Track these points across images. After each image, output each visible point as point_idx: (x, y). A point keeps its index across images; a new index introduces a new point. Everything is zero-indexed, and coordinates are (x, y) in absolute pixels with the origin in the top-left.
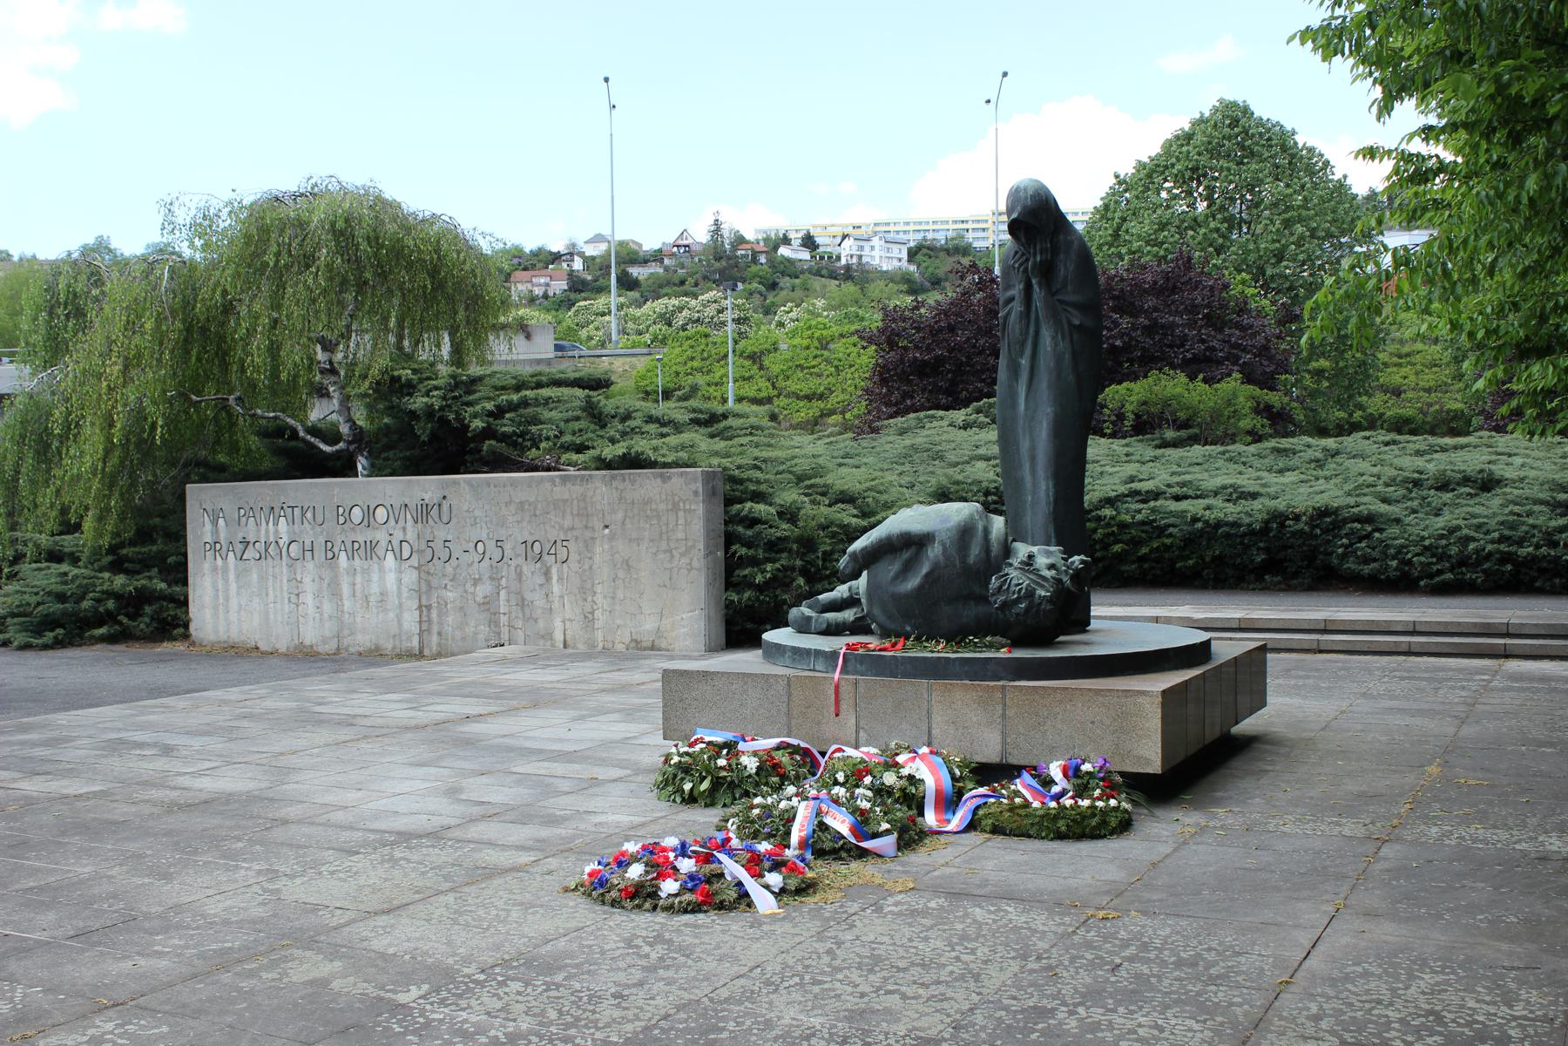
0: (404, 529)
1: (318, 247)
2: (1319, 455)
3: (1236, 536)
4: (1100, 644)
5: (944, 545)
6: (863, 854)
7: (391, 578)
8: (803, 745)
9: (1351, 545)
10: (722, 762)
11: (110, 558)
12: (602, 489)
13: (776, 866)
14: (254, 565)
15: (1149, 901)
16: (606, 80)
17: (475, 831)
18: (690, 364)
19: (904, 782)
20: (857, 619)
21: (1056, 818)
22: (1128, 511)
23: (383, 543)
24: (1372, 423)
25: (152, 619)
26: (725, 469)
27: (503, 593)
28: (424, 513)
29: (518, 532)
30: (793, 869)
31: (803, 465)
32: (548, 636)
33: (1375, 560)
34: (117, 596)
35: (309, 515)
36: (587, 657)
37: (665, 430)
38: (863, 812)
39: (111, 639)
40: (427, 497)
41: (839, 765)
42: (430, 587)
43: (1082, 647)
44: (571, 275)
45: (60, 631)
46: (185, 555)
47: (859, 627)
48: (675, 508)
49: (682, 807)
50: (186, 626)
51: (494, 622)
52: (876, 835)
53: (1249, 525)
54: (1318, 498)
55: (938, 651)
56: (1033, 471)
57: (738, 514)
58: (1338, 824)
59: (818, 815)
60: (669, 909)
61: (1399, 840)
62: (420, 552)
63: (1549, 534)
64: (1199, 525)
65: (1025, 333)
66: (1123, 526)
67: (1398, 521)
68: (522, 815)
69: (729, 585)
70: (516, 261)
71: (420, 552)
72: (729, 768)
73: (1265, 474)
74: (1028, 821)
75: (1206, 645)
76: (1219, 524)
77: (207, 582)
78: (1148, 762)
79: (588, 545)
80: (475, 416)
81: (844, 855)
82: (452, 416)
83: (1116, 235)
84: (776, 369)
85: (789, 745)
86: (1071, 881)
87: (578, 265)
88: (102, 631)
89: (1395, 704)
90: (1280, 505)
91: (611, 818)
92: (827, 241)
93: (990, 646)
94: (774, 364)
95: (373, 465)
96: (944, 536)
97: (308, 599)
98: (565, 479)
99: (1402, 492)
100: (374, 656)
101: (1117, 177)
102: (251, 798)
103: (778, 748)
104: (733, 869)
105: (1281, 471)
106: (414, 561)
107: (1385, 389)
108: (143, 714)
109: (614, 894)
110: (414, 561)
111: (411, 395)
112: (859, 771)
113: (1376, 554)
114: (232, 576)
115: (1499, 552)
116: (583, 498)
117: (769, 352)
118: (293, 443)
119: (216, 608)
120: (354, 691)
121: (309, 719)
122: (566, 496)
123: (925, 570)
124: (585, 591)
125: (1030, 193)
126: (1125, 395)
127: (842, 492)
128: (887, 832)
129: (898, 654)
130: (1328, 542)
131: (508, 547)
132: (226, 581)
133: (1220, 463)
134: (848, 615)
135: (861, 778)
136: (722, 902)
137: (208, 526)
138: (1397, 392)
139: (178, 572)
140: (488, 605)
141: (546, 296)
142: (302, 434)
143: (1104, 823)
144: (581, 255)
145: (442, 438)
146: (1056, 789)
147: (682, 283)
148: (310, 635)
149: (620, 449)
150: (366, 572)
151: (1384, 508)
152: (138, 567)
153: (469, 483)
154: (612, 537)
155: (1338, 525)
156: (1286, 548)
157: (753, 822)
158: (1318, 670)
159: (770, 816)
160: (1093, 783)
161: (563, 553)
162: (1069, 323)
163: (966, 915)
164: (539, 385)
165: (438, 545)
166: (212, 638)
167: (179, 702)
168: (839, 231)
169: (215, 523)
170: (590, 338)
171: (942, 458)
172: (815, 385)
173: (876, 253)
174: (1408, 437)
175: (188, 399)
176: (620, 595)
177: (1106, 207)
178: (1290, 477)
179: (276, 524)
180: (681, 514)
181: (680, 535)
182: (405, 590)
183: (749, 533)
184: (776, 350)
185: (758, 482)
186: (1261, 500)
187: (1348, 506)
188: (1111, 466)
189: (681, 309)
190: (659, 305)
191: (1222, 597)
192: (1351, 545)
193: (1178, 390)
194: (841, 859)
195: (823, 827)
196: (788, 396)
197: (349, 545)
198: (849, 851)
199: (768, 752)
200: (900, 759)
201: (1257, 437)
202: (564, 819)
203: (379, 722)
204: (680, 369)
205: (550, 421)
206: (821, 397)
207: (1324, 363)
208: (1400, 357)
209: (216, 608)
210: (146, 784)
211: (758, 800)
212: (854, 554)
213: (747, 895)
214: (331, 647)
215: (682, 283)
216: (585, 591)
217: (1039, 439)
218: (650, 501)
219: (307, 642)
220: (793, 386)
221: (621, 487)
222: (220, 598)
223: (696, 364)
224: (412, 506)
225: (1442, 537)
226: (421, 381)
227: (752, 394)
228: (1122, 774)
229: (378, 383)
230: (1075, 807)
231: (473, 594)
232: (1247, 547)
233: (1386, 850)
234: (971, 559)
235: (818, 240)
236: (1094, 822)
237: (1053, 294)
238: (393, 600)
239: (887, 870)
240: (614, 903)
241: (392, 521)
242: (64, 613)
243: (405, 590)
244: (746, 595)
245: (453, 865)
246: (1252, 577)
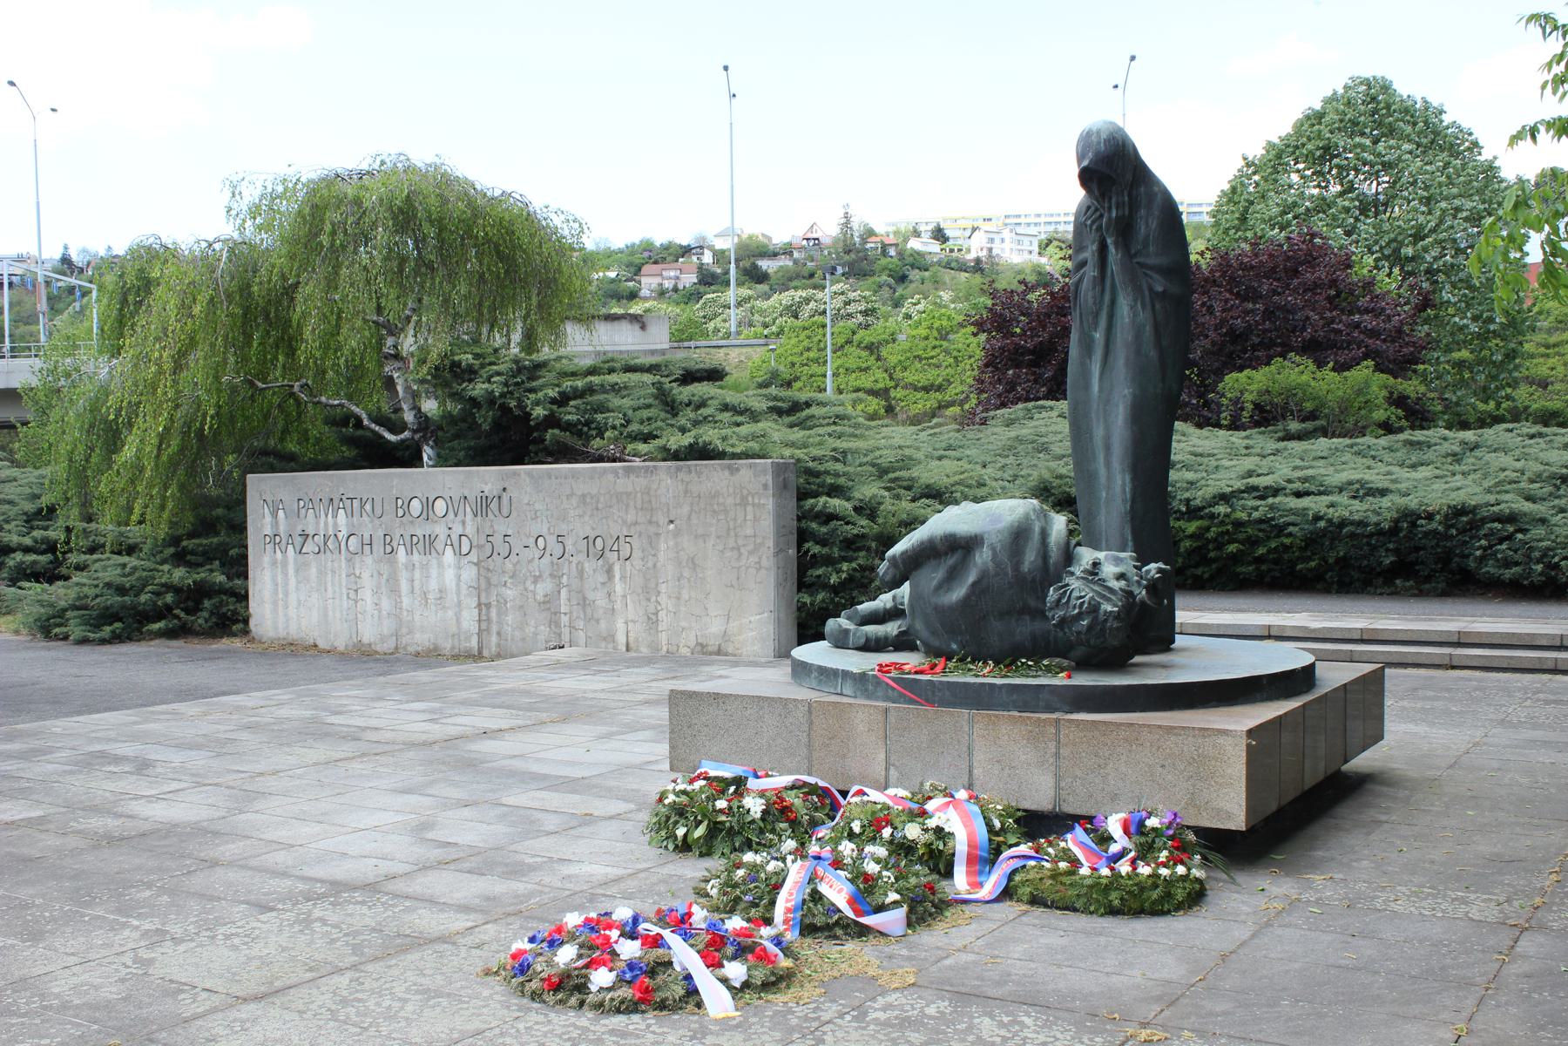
0: (464, 523)
1: (374, 225)
2: (1456, 449)
3: (1363, 536)
4: (1182, 667)
5: (993, 549)
6: (863, 931)
7: (450, 574)
8: (822, 784)
9: (1491, 547)
10: (721, 804)
11: (172, 550)
12: (667, 480)
13: (741, 952)
14: (315, 555)
15: (1211, 1014)
16: (726, 68)
17: (420, 885)
18: (806, 355)
19: (930, 837)
20: (901, 634)
21: (1107, 889)
22: (1244, 508)
23: (442, 537)
24: (1516, 416)
25: (212, 613)
26: (799, 460)
27: (564, 592)
28: (484, 505)
29: (579, 526)
30: (764, 957)
31: (888, 457)
32: (610, 638)
33: (1517, 564)
34: (177, 590)
35: (368, 507)
36: (648, 661)
37: (740, 419)
38: (867, 878)
39: (171, 634)
40: (487, 489)
41: (856, 812)
42: (489, 583)
43: (1164, 672)
44: (701, 267)
45: (118, 625)
46: (246, 547)
47: (903, 643)
48: (744, 503)
49: (674, 856)
50: (246, 621)
51: (554, 622)
52: (881, 908)
53: (1377, 524)
54: (1454, 495)
55: (986, 675)
56: (1108, 464)
57: (811, 509)
58: (1464, 901)
59: (811, 881)
60: (599, 1006)
61: (1542, 928)
62: (480, 547)
64: (1322, 524)
65: (1099, 302)
66: (1238, 524)
67: (1543, 521)
68: (484, 862)
69: (802, 585)
70: (646, 254)
71: (480, 547)
72: (729, 811)
73: (1396, 469)
74: (1072, 892)
75: (1309, 671)
76: (1343, 523)
77: (267, 576)
78: (1229, 816)
79: (652, 540)
80: (538, 403)
81: (839, 932)
82: (513, 404)
83: (1243, 219)
84: (893, 360)
85: (805, 784)
86: (1115, 979)
87: (708, 258)
88: (156, 626)
89: (1538, 734)
90: (1412, 502)
91: (586, 869)
92: (958, 233)
93: (1048, 669)
94: (892, 355)
95: (439, 456)
97: (367, 595)
98: (628, 471)
99: (1548, 489)
100: (430, 657)
102: (200, 831)
103: (793, 787)
104: (685, 956)
105: (1414, 466)
106: (473, 557)
107: (1530, 381)
108: (146, 721)
109: (535, 984)
110: (473, 557)
111: (470, 381)
112: (878, 820)
113: (1518, 557)
114: (291, 571)
116: (647, 491)
117: (887, 342)
118: (360, 432)
119: (275, 603)
120: (381, 699)
121: (316, 731)
122: (630, 489)
123: (971, 579)
124: (648, 590)
125: (1104, 136)
126: (1246, 384)
127: (928, 486)
128: (896, 904)
129: (935, 679)
130: (1465, 543)
131: (569, 543)
132: (286, 575)
133: (1347, 457)
134: (892, 628)
135: (879, 829)
136: (664, 1000)
137: (268, 518)
138: (1544, 384)
139: (238, 565)
140: (549, 604)
141: (675, 290)
142: (366, 422)
143: (1168, 895)
144: (711, 248)
145: (510, 430)
146: (1114, 848)
147: (812, 275)
148: (369, 633)
149: (687, 440)
150: (425, 567)
151: (1527, 506)
152: (200, 559)
153: (529, 473)
154: (677, 533)
155: (1475, 525)
156: (1417, 549)
157: (736, 886)
158: (1448, 690)
159: (754, 880)
160: (1159, 843)
161: (625, 551)
162: (1151, 289)
163: (970, 1027)
164: (611, 371)
165: (497, 540)
166: (271, 634)
167: (189, 708)
168: (969, 225)
169: (275, 515)
170: (717, 330)
171: (1046, 450)
172: (933, 376)
173: (1007, 245)
174: (1555, 429)
175: (252, 384)
176: (685, 595)
177: (1234, 189)
178: (1424, 472)
179: (335, 516)
180: (749, 509)
181: (749, 532)
182: (464, 587)
183: (824, 529)
184: (894, 341)
185: (837, 475)
186: (1390, 497)
187: (1488, 504)
188: (1213, 462)
189: (808, 300)
190: (786, 298)
191: (1346, 603)
192: (1491, 547)
193: (1304, 377)
194: (836, 937)
195: (816, 897)
196: (905, 387)
197: (408, 538)
198: (845, 927)
199: (778, 793)
200: (930, 806)
201: (1387, 428)
202: (533, 868)
203: (389, 736)
204: (795, 359)
205: (619, 409)
206: (939, 388)
207: (1464, 354)
208: (1548, 347)
209: (275, 603)
210: (95, 810)
211: (749, 857)
212: (894, 557)
213: (696, 992)
214: (389, 645)
215: (812, 275)
216: (648, 590)
217: (1114, 426)
218: (717, 495)
219: (366, 640)
220: (910, 377)
221: (687, 479)
222: (282, 594)
223: (812, 355)
224: (471, 498)
226: (483, 366)
227: (868, 385)
228: (1198, 831)
229: (437, 368)
230: (1134, 874)
231: (534, 593)
232: (1374, 548)
233: (1526, 944)
234: (1026, 567)
235: (948, 233)
236: (1155, 895)
237: (1132, 257)
238: (451, 597)
239: (893, 954)
240: (534, 996)
241: (451, 515)
242: (123, 607)
243: (464, 587)
244: (820, 597)
245: (374, 930)
246: (1380, 580)
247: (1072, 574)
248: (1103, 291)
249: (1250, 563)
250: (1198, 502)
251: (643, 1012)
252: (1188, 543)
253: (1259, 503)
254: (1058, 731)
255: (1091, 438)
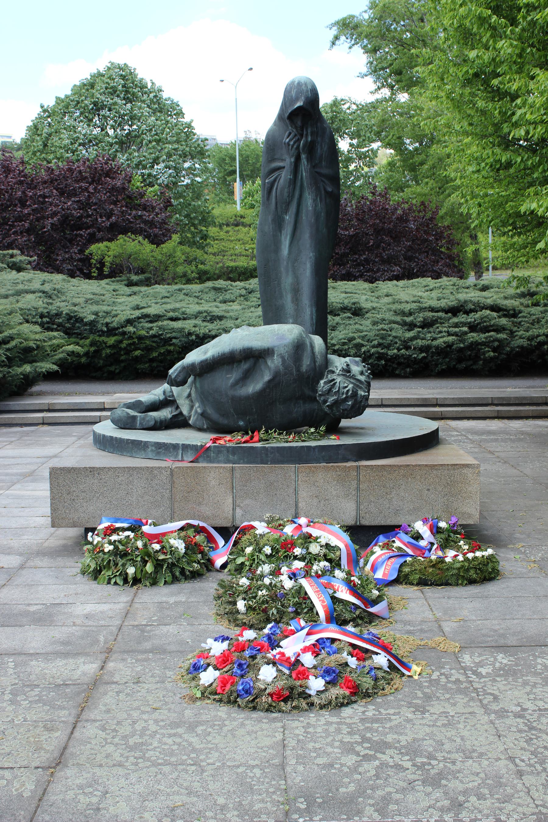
2: (244, 292)
5: (283, 357)
22: (143, 328)
63: (405, 341)
65: (291, 196)
66: (140, 338)
78: (470, 516)
81: (360, 622)
96: (282, 351)
101: (42, 107)
115: (378, 353)
123: (267, 377)
126: (104, 250)
133: (182, 297)
134: (166, 413)
146: (423, 543)
225: (344, 344)
234: (304, 368)
240: (269, 709)
247: (333, 372)
248: (294, 189)
249: (145, 363)
250: (115, 325)
251: (355, 702)
252: (108, 351)
253: (150, 325)
254: (359, 474)
255: (279, 284)
